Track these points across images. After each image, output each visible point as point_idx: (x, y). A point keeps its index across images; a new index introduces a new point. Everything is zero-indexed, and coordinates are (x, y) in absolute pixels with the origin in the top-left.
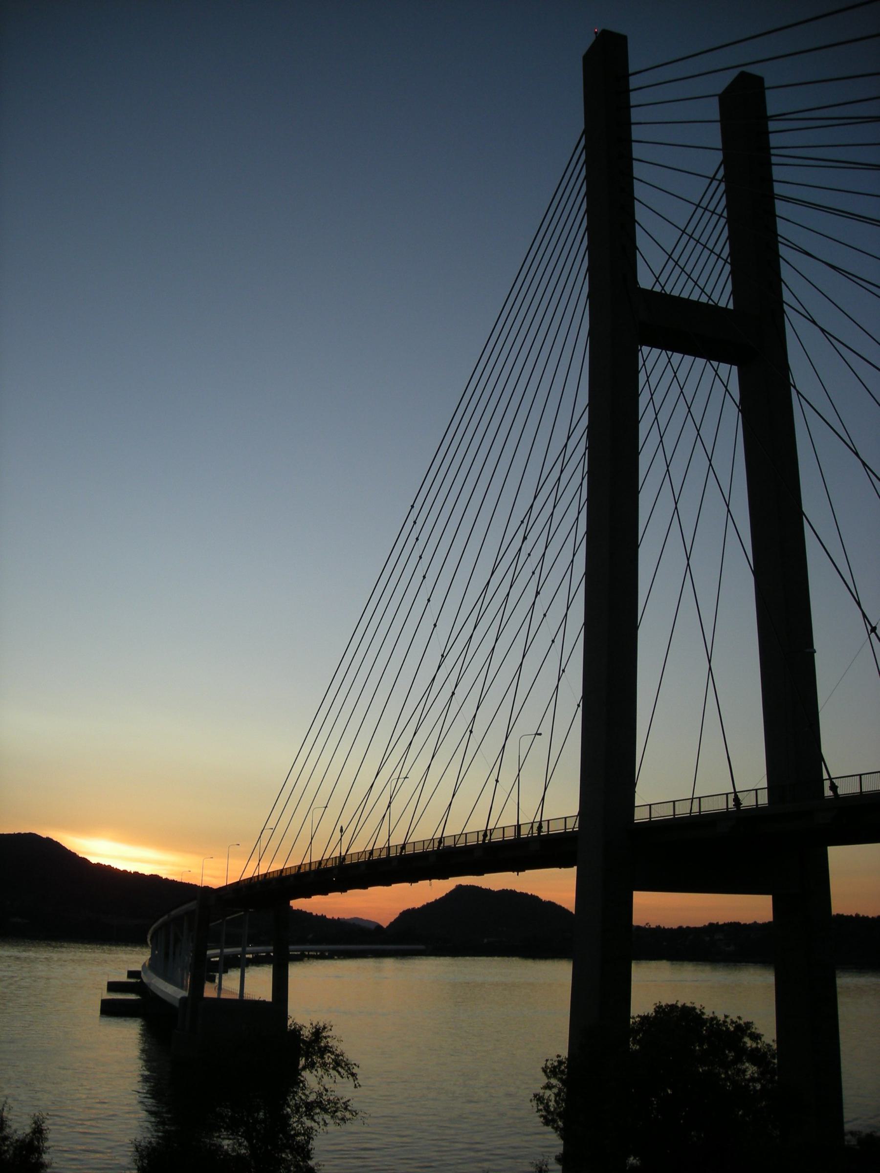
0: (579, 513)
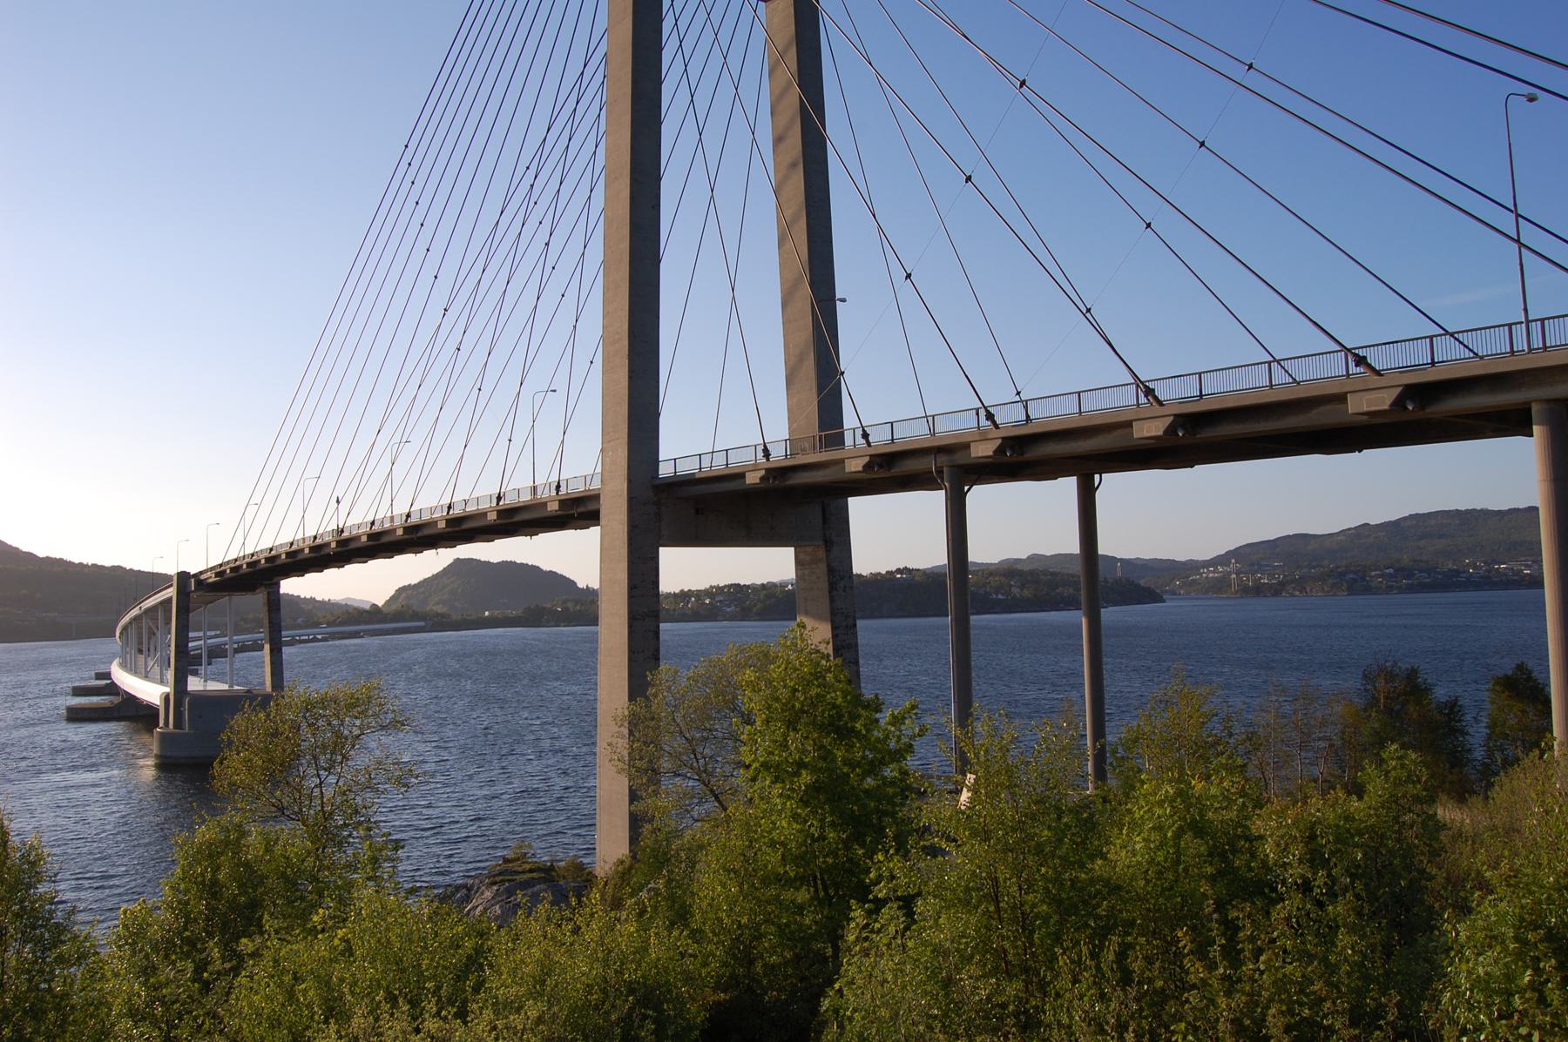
0: (601, 110)
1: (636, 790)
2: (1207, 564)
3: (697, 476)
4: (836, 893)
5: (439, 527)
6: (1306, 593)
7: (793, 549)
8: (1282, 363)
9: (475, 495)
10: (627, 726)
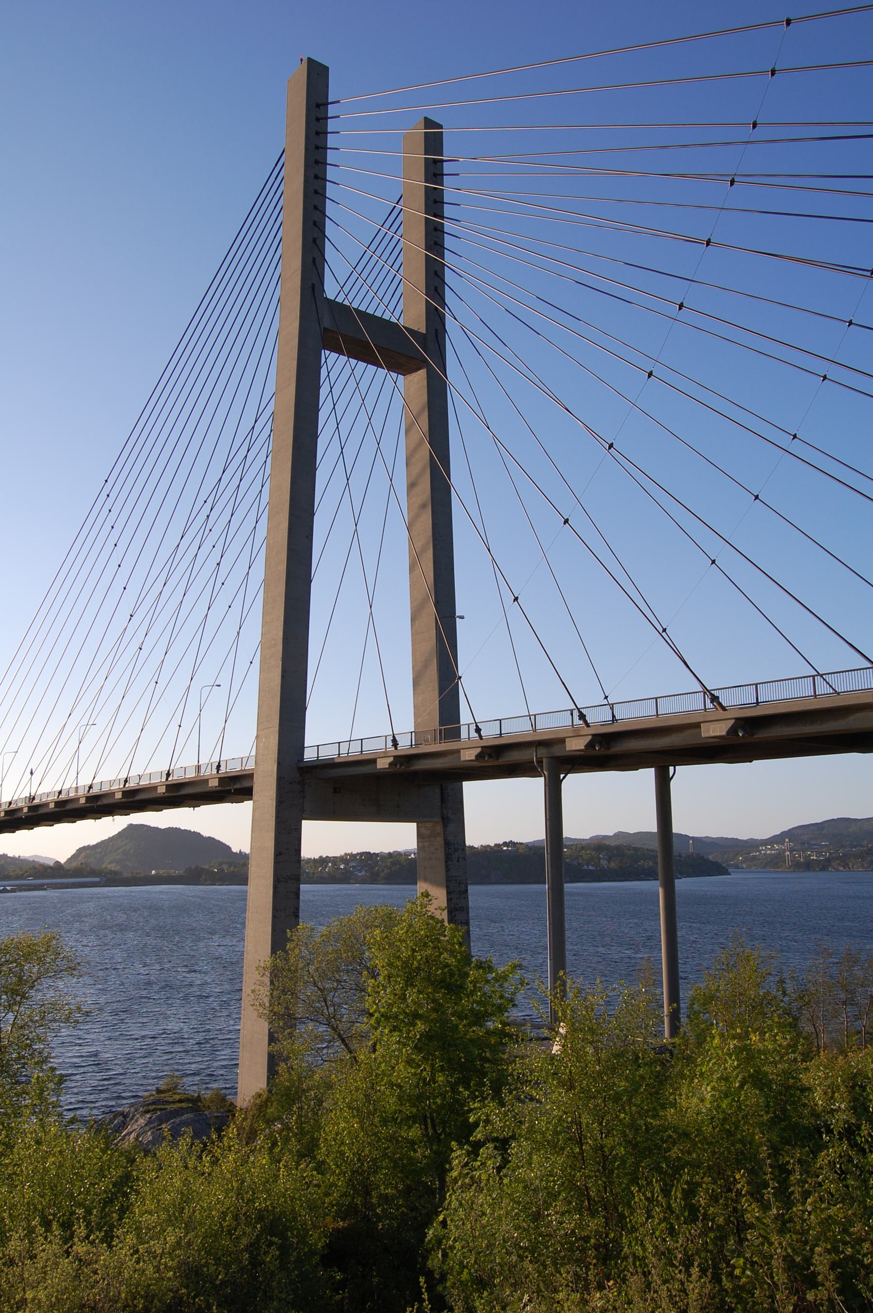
0: (267, 457)
1: (274, 1032)
2: (765, 842)
3: (336, 761)
4: (444, 1131)
5: (116, 797)
6: (849, 868)
7: (415, 824)
8: (824, 676)
9: (148, 771)
10: (269, 975)
